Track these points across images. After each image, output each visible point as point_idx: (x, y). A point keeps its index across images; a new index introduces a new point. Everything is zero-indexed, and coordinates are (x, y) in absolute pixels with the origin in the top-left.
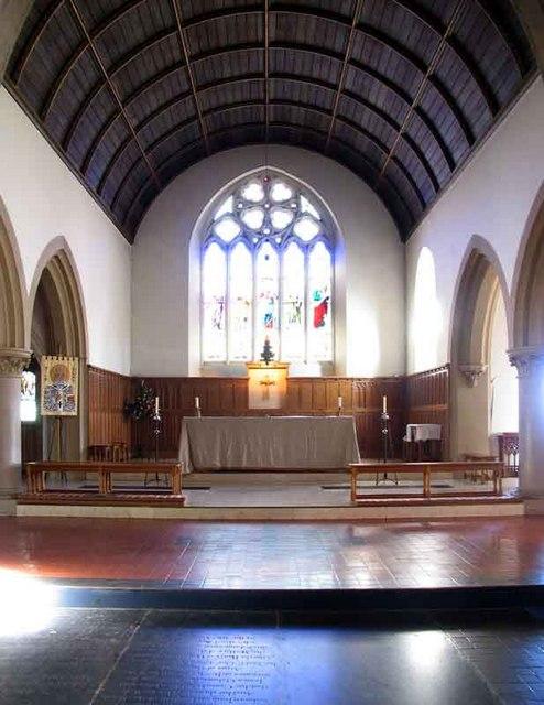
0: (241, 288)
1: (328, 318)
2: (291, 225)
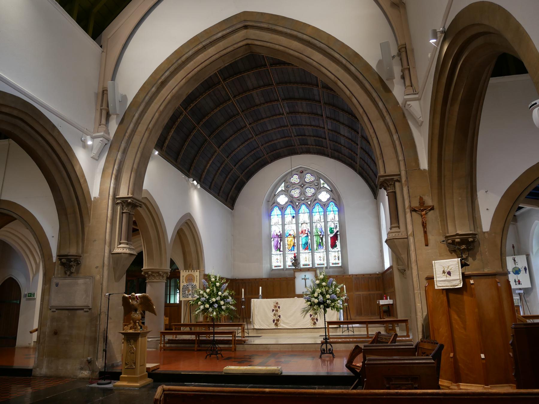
0: (291, 229)
1: (338, 243)
2: (314, 194)
